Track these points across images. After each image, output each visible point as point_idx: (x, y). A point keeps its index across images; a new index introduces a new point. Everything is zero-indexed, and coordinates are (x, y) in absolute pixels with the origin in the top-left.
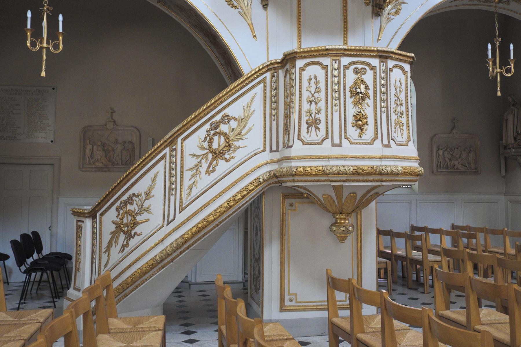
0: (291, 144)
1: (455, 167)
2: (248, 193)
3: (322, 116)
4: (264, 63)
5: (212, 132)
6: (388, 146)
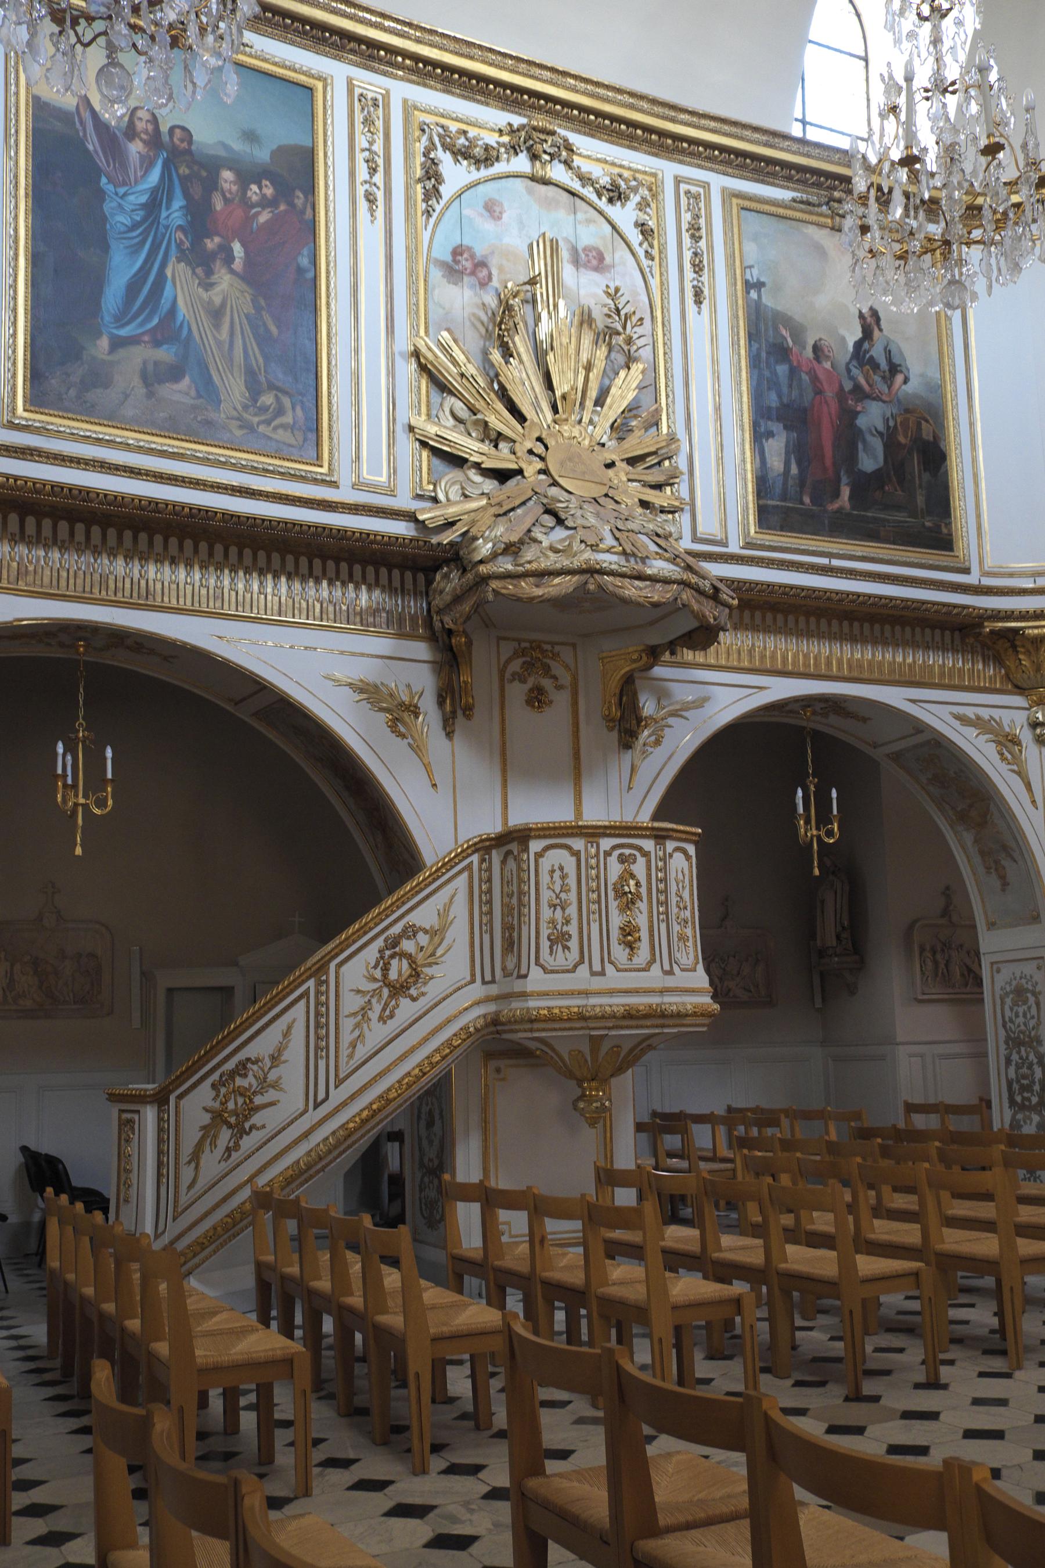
0: (523, 971)
1: (731, 994)
2: (451, 1052)
3: (573, 929)
4: (469, 840)
5: (388, 953)
6: (670, 972)
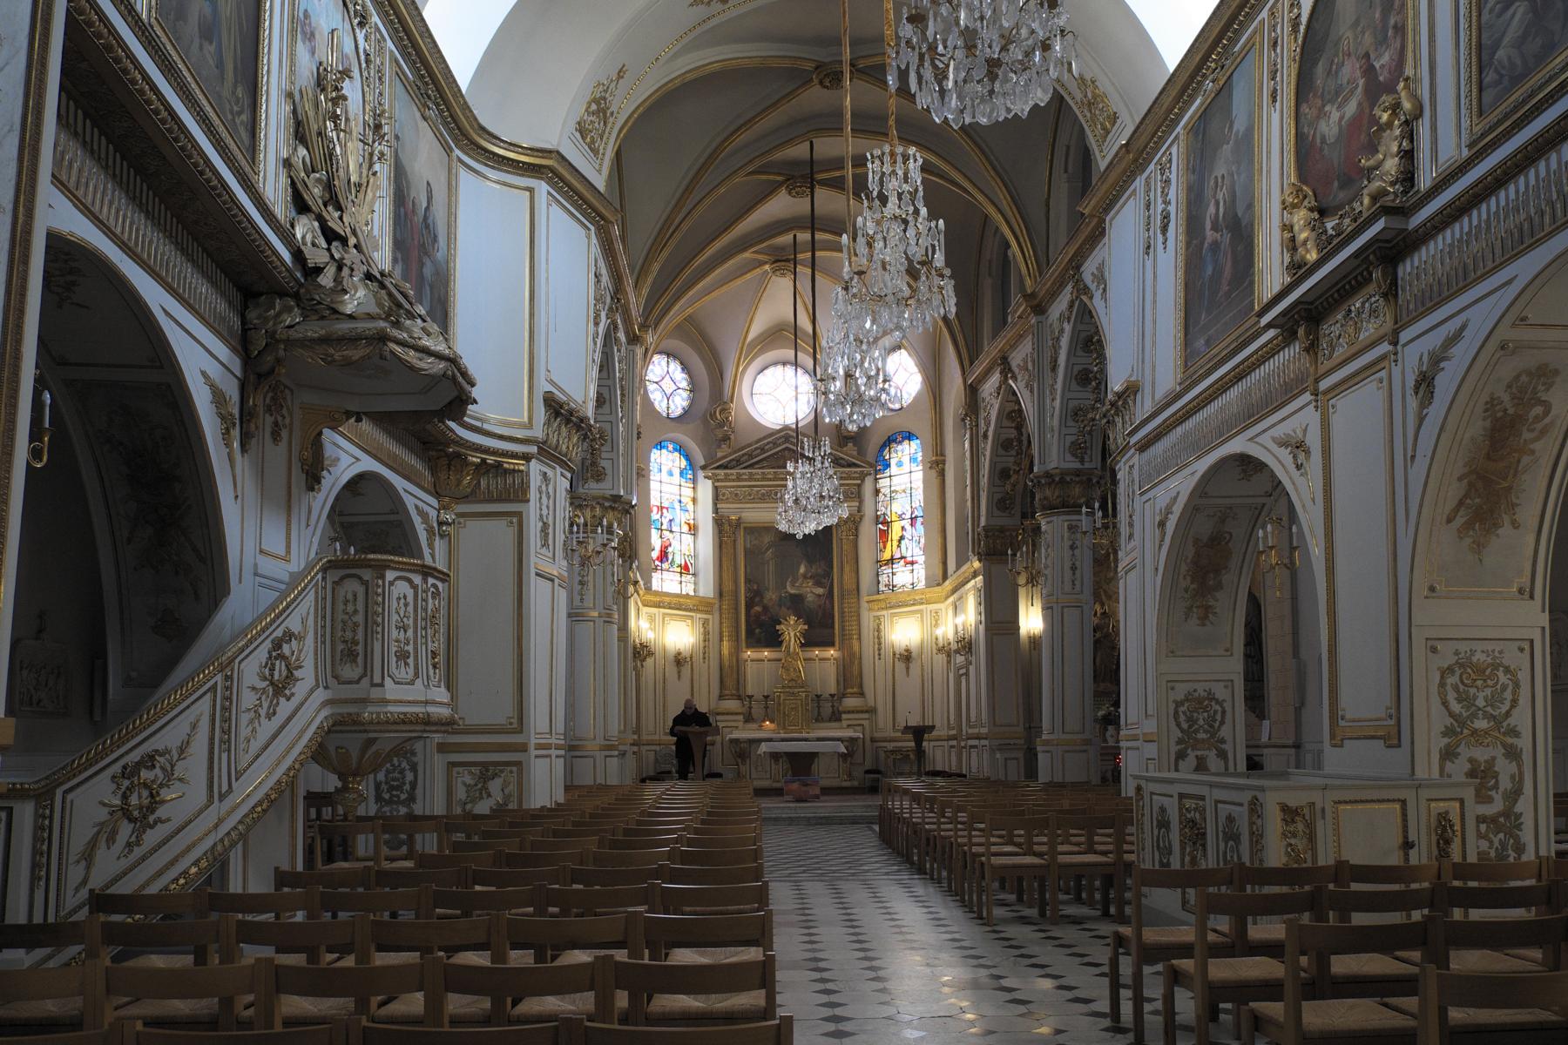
3: (360, 648)
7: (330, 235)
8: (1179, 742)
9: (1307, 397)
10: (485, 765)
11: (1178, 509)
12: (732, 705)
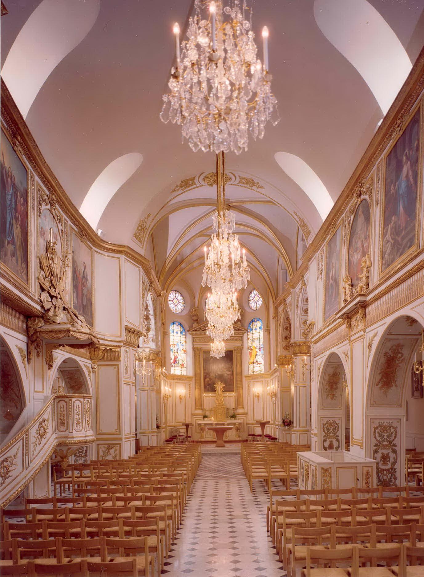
3: (65, 422)
7: (52, 297)
8: (325, 436)
9: (347, 341)
10: (109, 445)
11: (322, 365)
12: (200, 412)
